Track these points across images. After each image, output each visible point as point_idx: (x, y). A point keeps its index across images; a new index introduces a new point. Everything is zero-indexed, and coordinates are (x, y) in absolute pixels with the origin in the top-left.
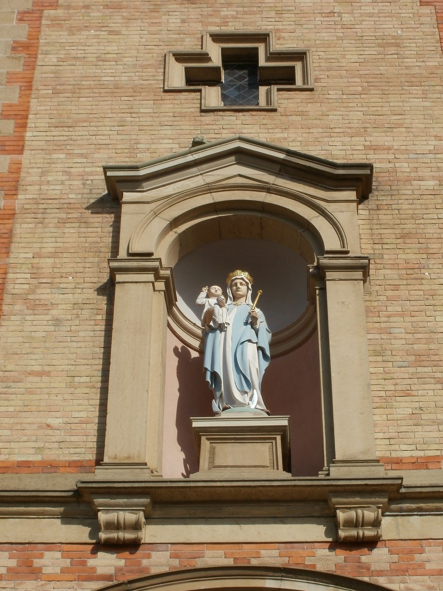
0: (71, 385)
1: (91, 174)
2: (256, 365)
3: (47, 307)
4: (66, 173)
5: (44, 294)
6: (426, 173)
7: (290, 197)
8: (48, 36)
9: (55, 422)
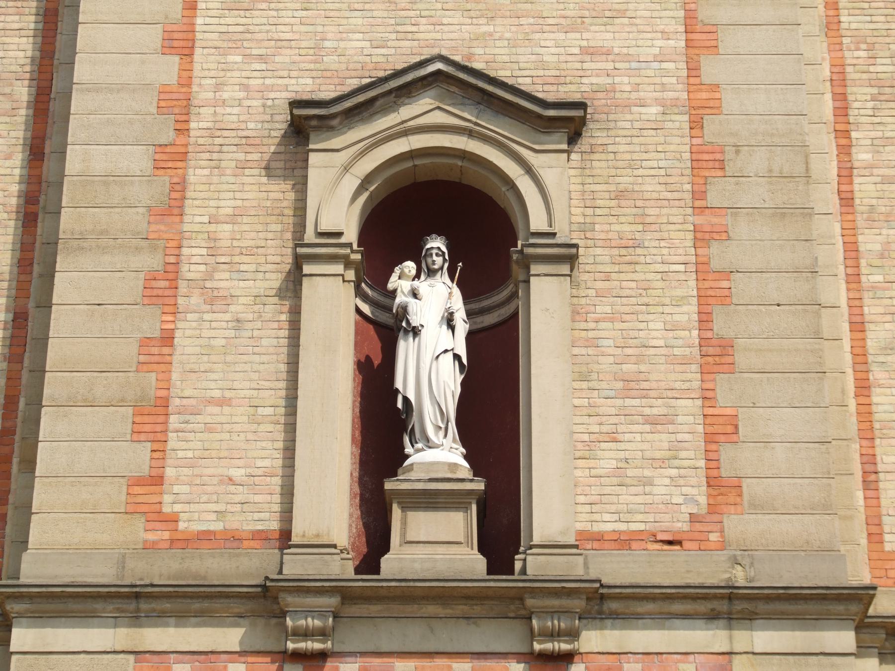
0: (254, 420)
1: (272, 88)
2: (448, 382)
3: (229, 299)
4: (245, 88)
5: (223, 281)
6: (647, 94)
7: (495, 150)
9: (237, 473)
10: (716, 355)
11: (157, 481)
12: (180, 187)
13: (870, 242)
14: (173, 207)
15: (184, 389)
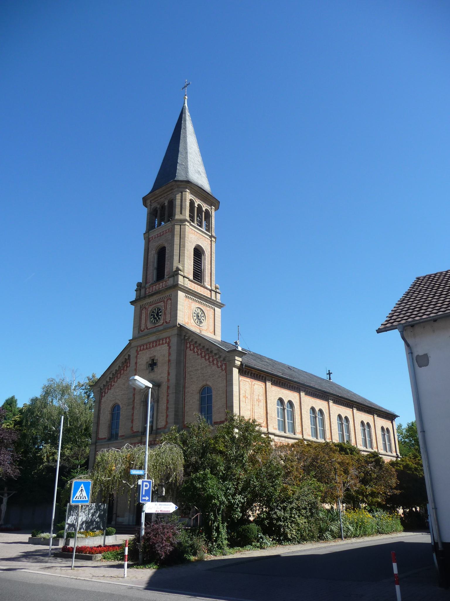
8: (138, 360)
10: (167, 408)
11: (132, 427)
12: (134, 398)
13: (186, 391)
14: (134, 401)
15: (135, 418)
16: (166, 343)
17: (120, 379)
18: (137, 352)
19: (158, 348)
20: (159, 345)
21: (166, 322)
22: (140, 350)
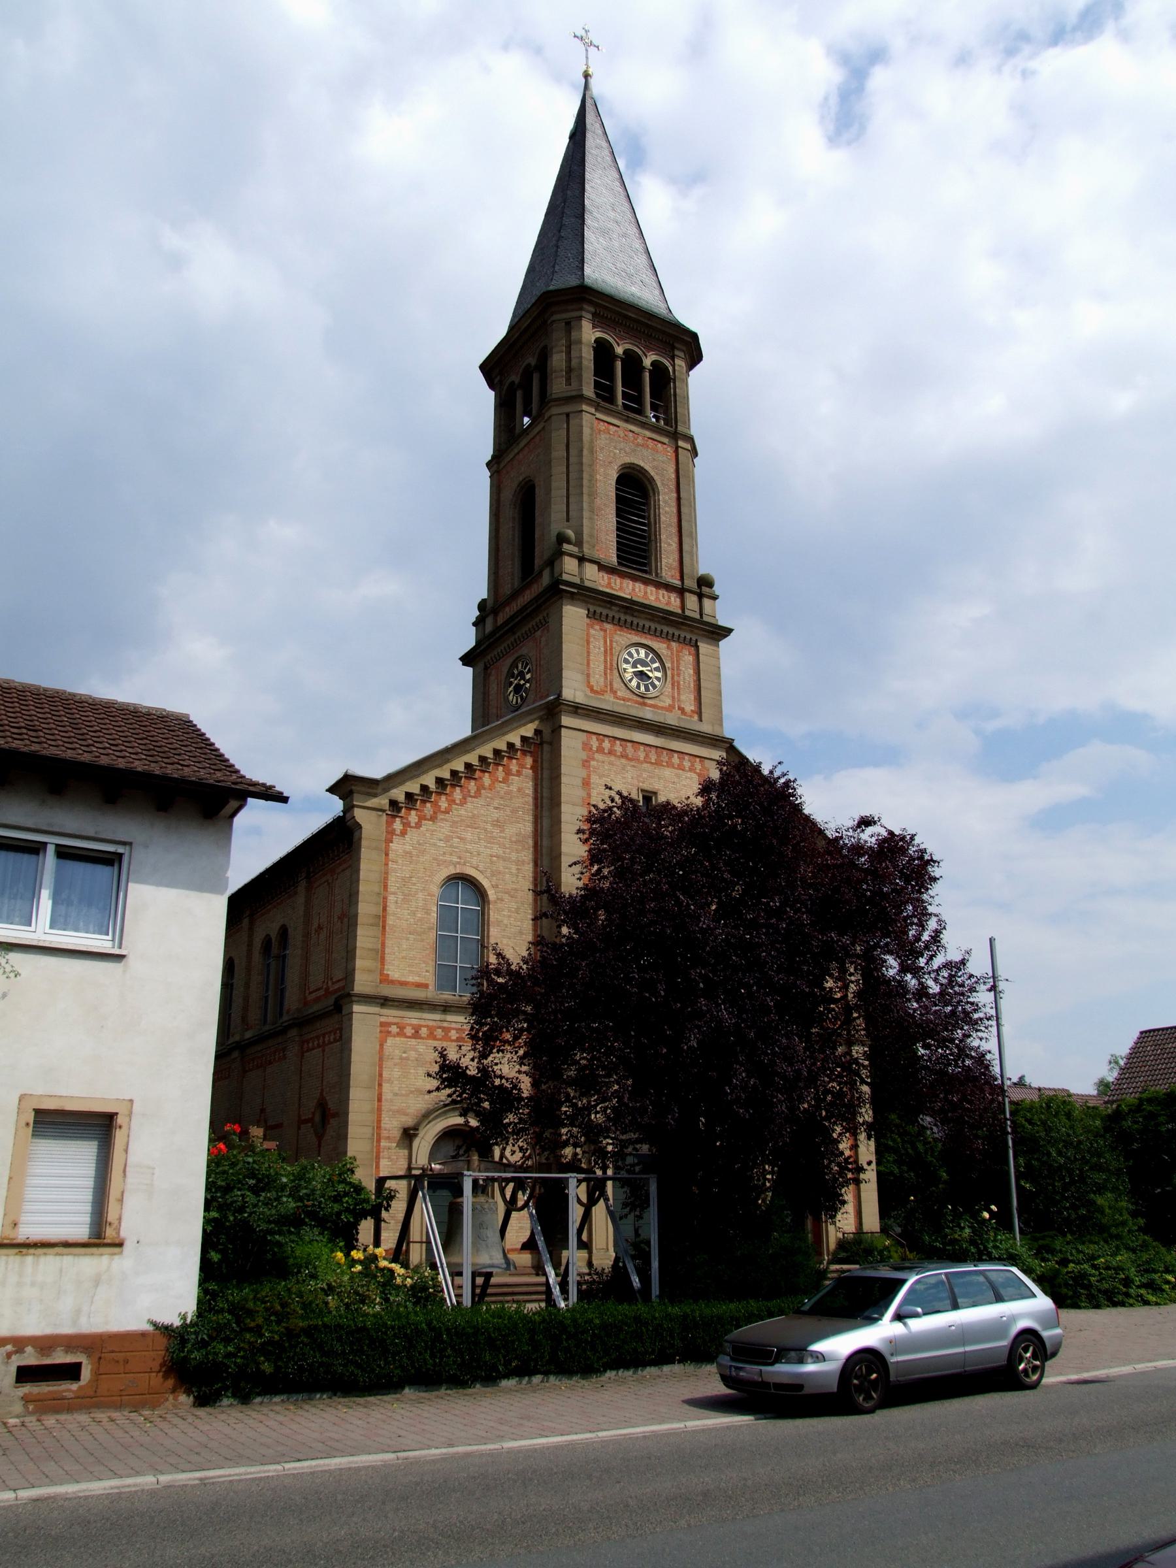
16: (692, 769)
17: (480, 801)
18: (586, 746)
19: (668, 773)
20: (670, 765)
21: (682, 709)
22: (600, 750)
